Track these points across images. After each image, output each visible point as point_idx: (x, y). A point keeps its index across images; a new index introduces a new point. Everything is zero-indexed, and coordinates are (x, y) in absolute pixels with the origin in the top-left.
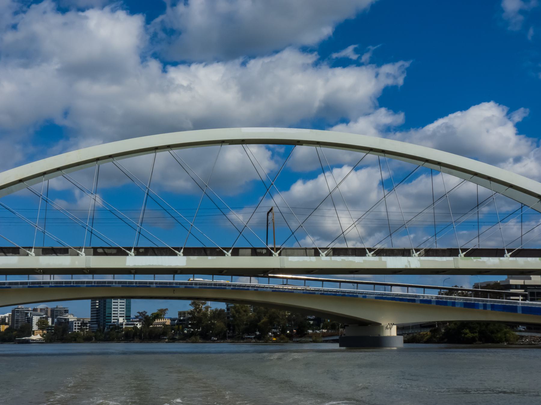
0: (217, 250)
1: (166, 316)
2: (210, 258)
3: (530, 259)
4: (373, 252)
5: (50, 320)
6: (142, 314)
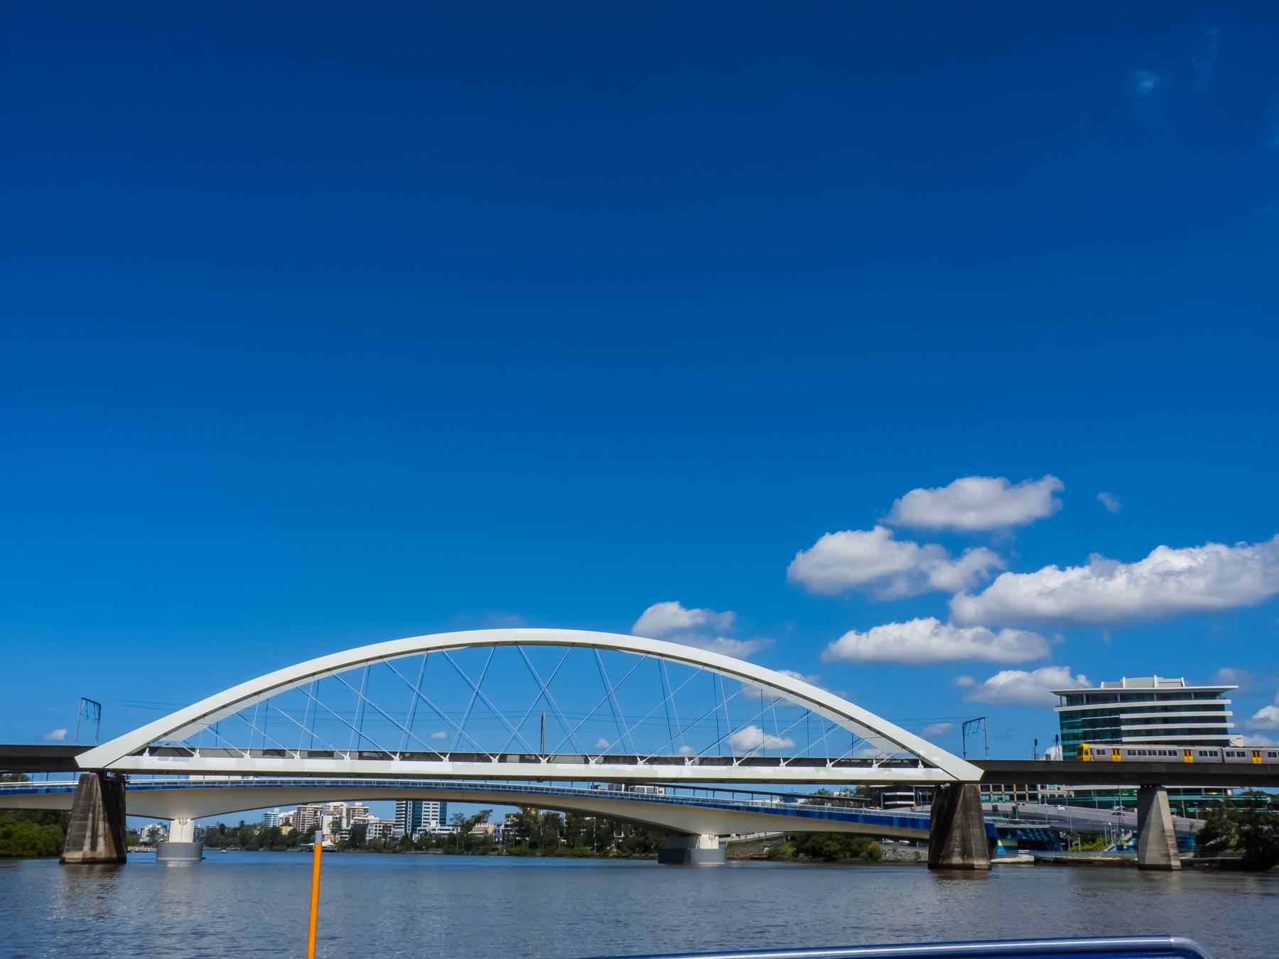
2: (476, 764)
3: (894, 770)
5: (344, 822)
6: (458, 817)
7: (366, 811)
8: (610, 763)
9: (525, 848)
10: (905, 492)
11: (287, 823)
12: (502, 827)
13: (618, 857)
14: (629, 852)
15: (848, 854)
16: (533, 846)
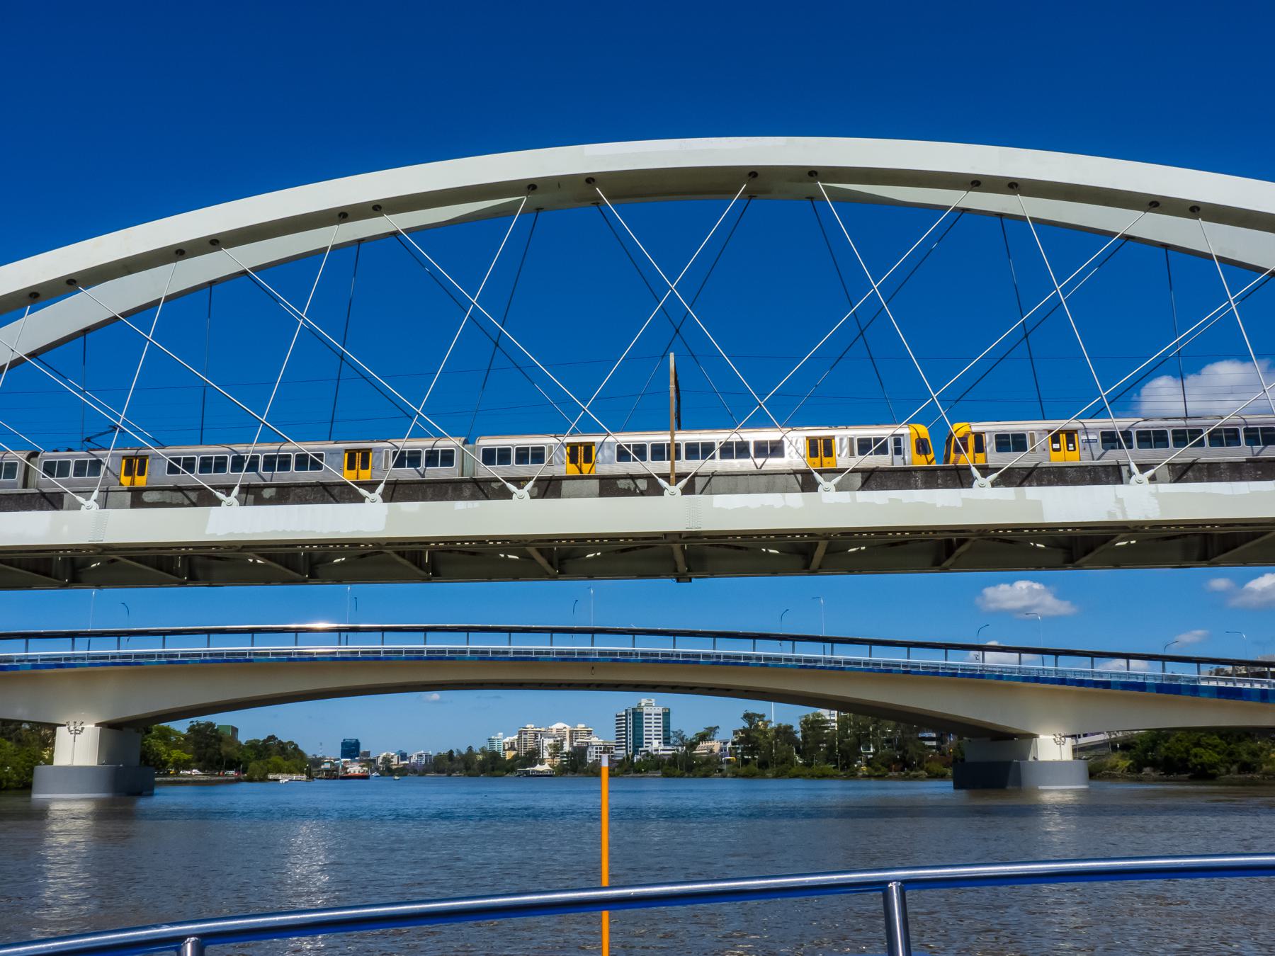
0: (494, 485)
1: (717, 737)
2: (460, 505)
4: (995, 475)
7: (589, 733)
8: (882, 487)
9: (753, 768)
10: (1203, 366)
11: (512, 748)
12: (729, 745)
13: (869, 776)
14: (884, 769)
15: (1235, 768)
16: (763, 765)
